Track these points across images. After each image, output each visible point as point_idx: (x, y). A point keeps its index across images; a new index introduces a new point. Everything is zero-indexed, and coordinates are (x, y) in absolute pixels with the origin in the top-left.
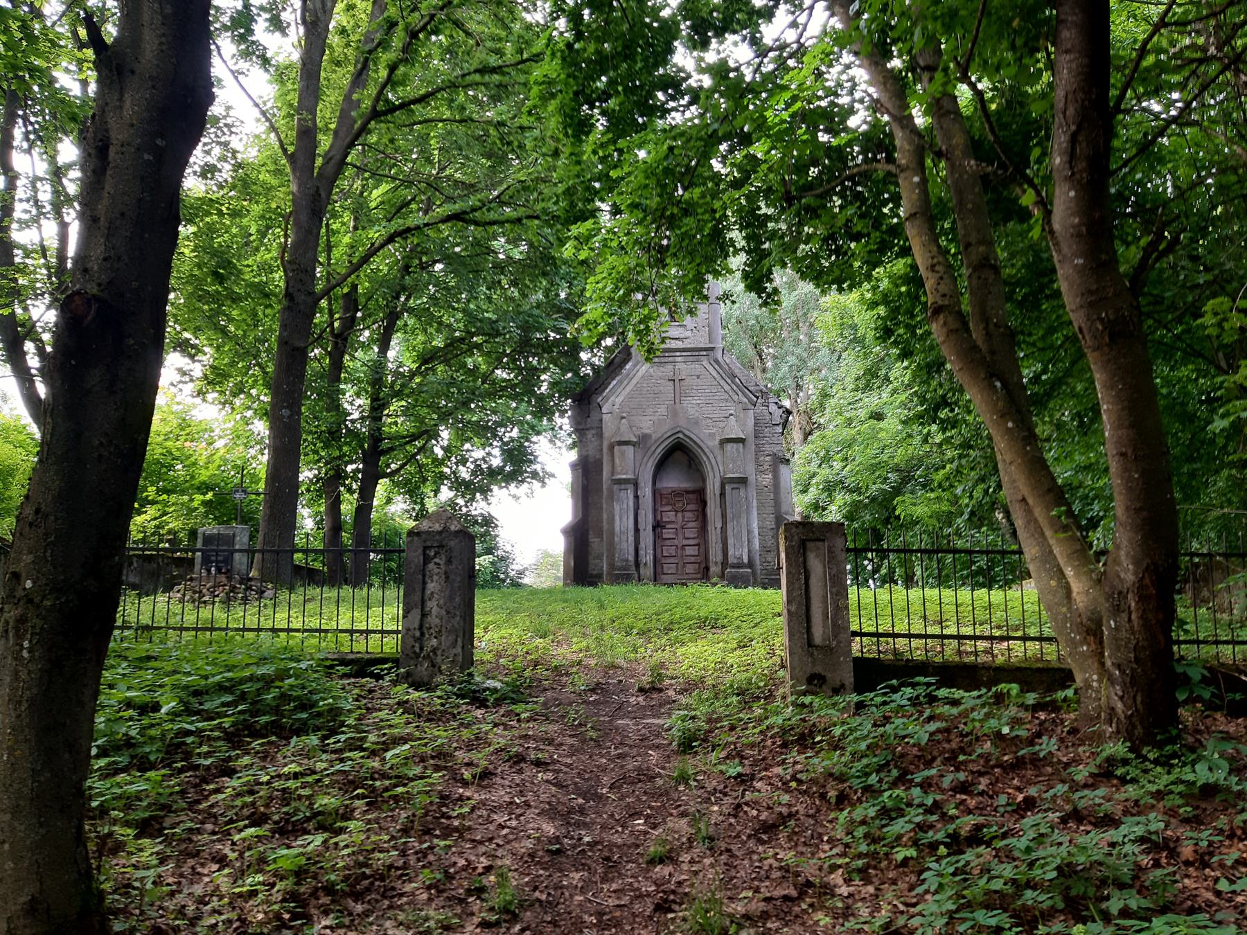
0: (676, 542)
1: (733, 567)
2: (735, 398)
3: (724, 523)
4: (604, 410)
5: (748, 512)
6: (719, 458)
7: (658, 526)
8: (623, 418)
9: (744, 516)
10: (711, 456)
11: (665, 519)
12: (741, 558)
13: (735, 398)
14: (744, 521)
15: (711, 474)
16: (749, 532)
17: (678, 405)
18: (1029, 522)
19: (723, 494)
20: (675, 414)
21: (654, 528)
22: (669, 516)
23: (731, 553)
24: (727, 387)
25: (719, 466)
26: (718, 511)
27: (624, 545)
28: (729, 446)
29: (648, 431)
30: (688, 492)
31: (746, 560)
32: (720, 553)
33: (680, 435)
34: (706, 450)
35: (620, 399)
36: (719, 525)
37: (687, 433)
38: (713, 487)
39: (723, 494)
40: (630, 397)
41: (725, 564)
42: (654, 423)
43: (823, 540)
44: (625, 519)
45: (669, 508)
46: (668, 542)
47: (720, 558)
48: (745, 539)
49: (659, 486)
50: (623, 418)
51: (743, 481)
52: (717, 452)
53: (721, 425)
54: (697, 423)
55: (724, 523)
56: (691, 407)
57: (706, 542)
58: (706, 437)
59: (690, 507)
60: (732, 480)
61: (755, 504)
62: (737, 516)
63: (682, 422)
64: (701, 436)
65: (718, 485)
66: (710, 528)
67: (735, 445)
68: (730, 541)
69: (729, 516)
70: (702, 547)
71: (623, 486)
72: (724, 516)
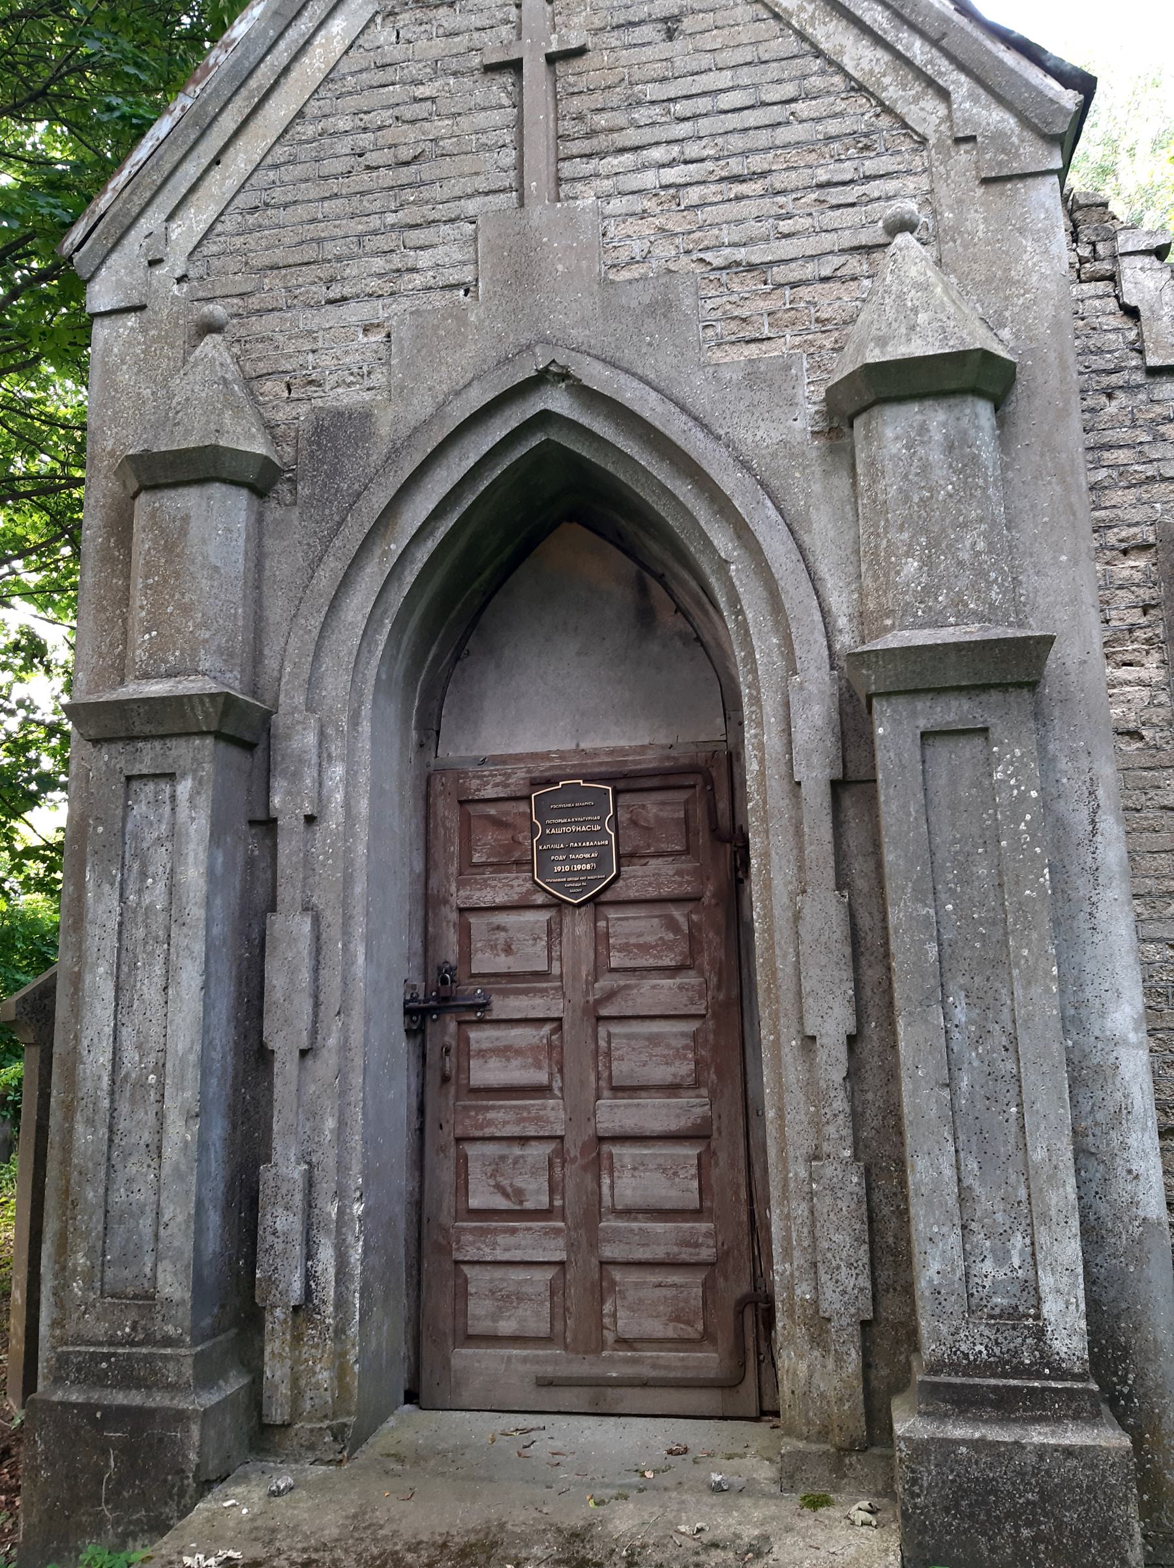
0: (553, 1114)
1: (965, 1402)
2: (926, 114)
3: (873, 1003)
4: (100, 296)
5: (1067, 918)
6: (824, 531)
7: (438, 1006)
8: (210, 327)
9: (1031, 948)
10: (765, 521)
11: (485, 962)
12: (1022, 1314)
13: (926, 114)
14: (1038, 1002)
15: (765, 646)
16: (1084, 1075)
17: (539, 213)
18: (351, 917)
19: (852, 786)
20: (521, 268)
21: (419, 1016)
22: (513, 940)
23: (935, 1264)
24: (860, 57)
25: (813, 580)
26: (824, 913)
27: (137, 1182)
28: (893, 431)
29: (349, 397)
30: (626, 781)
31: (1068, 1337)
32: (843, 1240)
33: (557, 401)
34: (729, 480)
35: (196, 219)
36: (832, 1021)
37: (595, 375)
38: (785, 738)
39: (852, 786)
40: (254, 204)
41: (885, 1330)
42: (397, 358)
43: (170, 777)
44: (148, 989)
45: (514, 886)
46: (502, 1118)
47: (843, 1288)
48: (1051, 1147)
49: (456, 748)
50: (210, 327)
51: (1011, 670)
52: (815, 492)
53: (832, 301)
54: (662, 308)
55: (873, 1003)
56: (621, 219)
57: (749, 1111)
58: (729, 406)
59: (639, 879)
60: (925, 674)
61: (1111, 849)
62: (980, 960)
63: (571, 323)
64: (698, 390)
65: (814, 718)
66: (776, 1035)
67: (936, 419)
68: (930, 1168)
69: (911, 951)
70: (727, 1151)
71: (148, 757)
72: (866, 949)
